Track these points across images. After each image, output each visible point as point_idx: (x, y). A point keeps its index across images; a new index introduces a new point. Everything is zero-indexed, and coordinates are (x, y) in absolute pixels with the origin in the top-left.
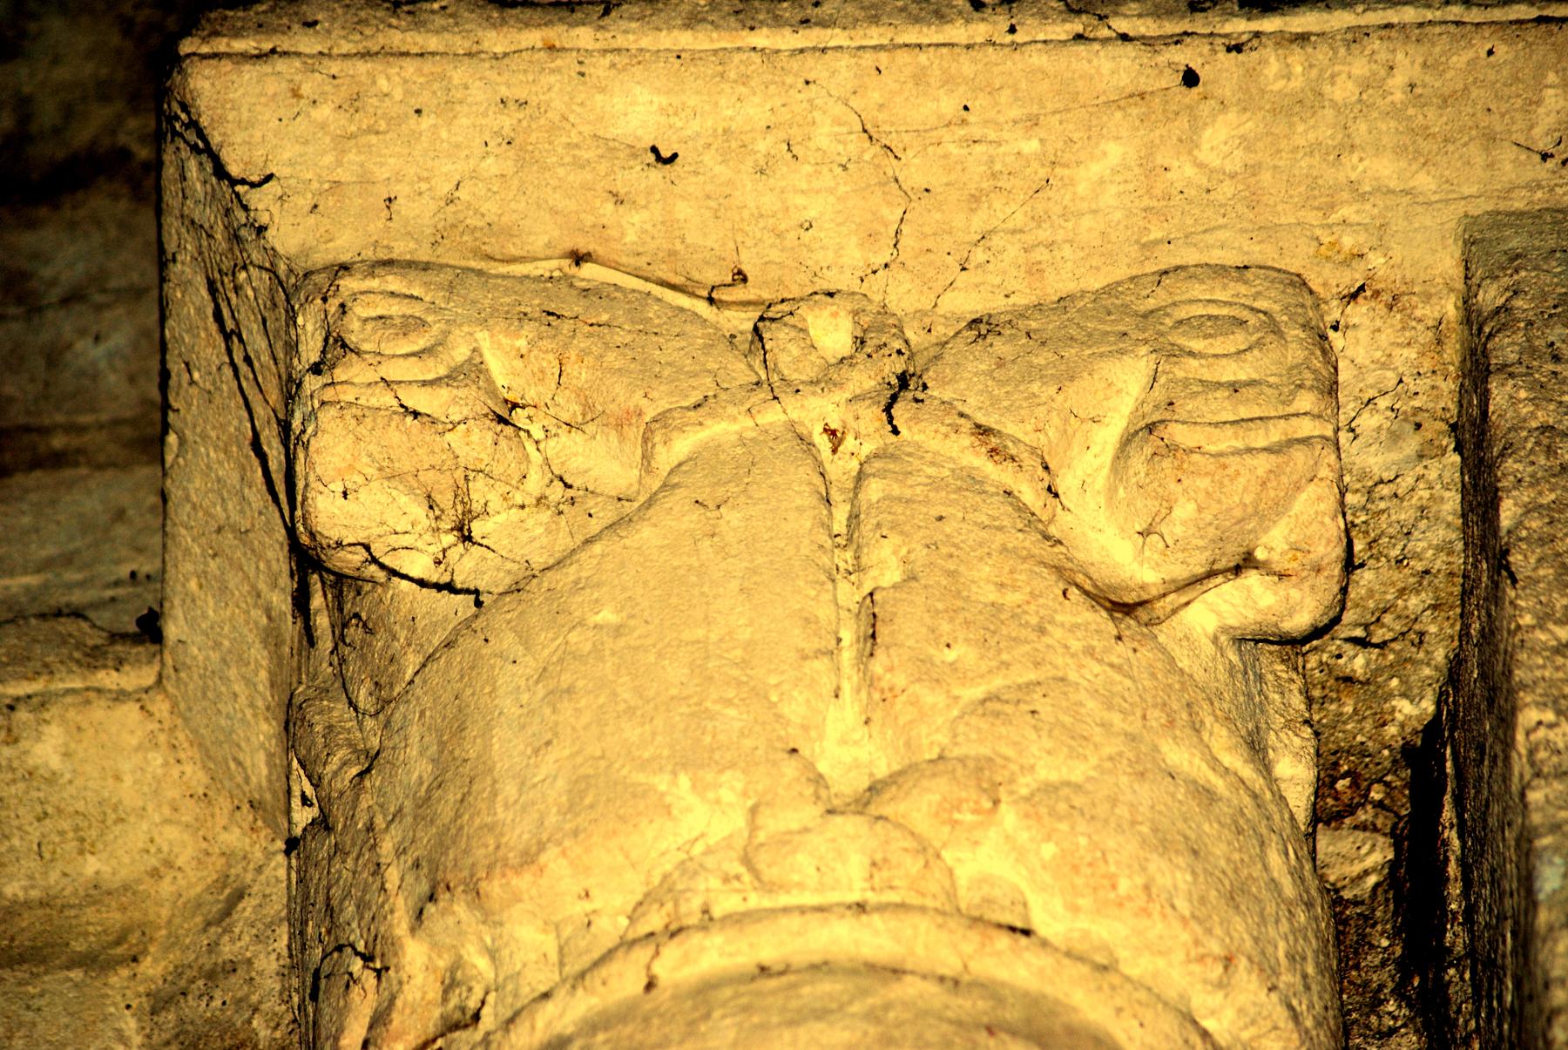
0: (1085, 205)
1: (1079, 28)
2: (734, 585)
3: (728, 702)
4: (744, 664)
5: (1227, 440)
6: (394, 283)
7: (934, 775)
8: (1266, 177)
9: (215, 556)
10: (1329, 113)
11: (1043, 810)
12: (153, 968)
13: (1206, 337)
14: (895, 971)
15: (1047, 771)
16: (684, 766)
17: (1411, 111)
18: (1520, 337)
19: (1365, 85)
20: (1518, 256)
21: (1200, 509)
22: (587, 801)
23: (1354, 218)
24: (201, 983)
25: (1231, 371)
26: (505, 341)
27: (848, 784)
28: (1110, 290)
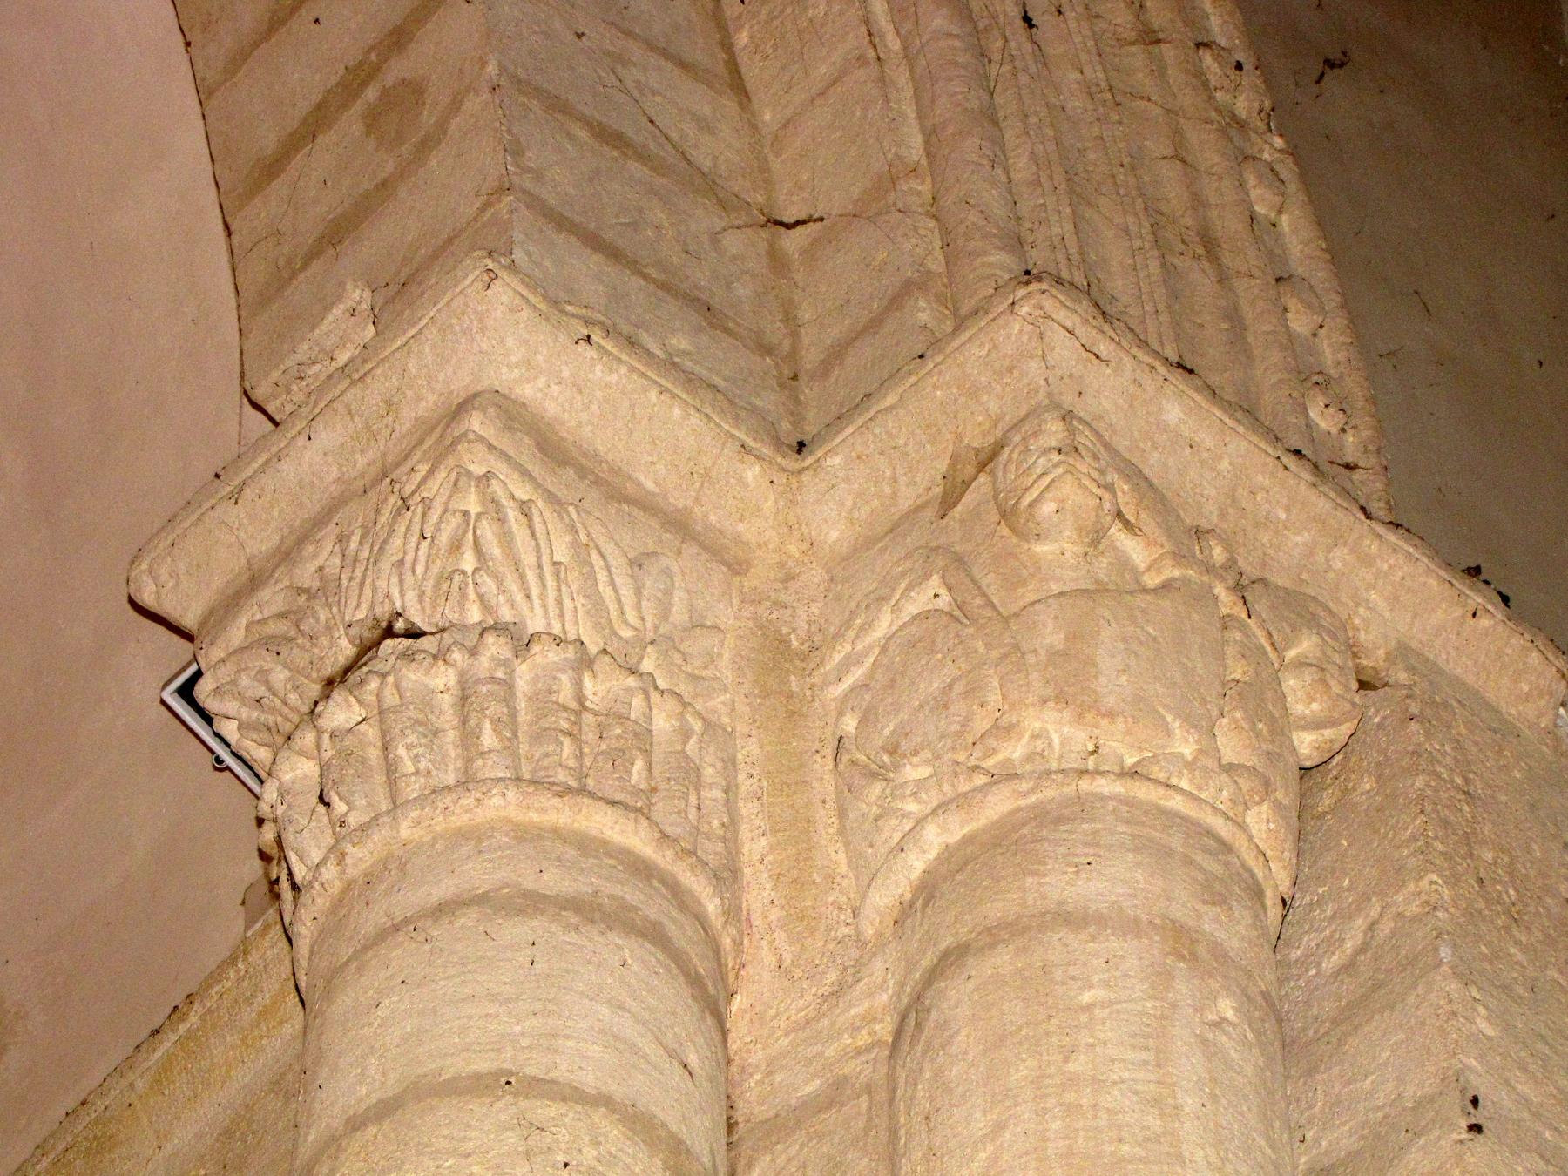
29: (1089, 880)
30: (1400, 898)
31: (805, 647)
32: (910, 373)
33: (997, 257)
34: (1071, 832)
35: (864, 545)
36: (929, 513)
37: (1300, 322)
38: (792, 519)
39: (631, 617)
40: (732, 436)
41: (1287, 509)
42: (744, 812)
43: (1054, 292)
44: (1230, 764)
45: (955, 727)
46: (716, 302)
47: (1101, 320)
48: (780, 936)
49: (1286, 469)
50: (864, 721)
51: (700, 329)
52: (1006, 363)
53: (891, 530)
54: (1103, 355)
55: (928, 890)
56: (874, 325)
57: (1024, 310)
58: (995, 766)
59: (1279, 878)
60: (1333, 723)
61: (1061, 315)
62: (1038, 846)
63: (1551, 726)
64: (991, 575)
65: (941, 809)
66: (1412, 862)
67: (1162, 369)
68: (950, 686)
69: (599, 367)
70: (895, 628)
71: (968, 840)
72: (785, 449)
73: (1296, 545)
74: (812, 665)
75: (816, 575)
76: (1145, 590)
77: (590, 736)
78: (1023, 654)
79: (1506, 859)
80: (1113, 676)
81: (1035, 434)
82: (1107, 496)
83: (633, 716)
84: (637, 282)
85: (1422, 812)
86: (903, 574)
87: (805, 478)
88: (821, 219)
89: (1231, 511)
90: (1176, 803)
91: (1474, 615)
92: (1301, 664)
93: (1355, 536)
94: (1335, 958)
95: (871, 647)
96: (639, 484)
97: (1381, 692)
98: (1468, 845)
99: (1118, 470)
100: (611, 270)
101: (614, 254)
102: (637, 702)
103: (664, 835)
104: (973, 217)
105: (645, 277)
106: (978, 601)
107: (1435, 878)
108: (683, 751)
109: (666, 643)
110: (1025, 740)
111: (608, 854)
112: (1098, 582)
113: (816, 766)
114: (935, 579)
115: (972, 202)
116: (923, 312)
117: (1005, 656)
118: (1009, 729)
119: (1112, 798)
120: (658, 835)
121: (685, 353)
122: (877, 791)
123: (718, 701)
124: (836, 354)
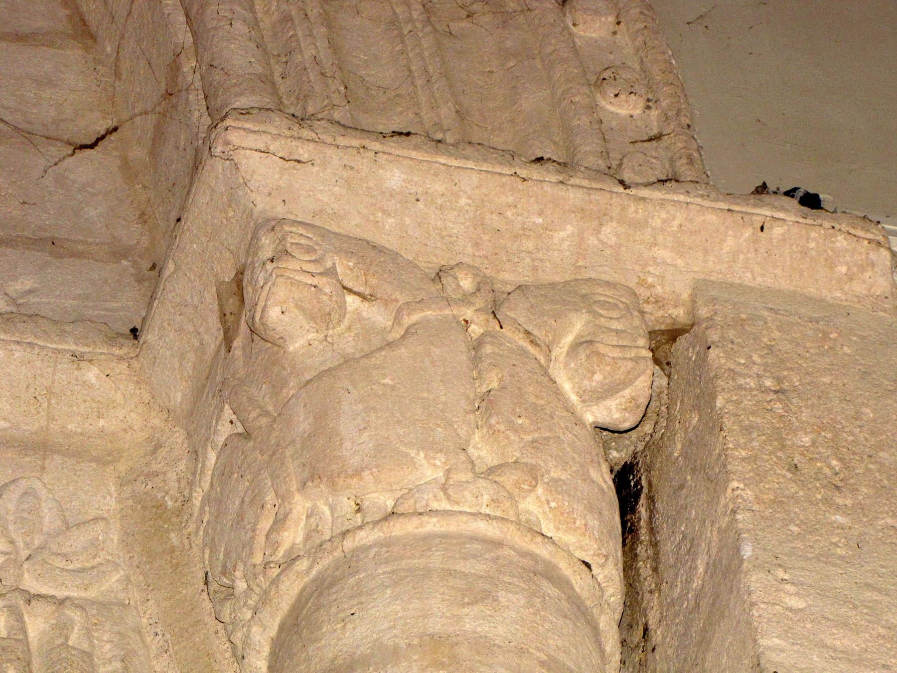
0: (555, 247)
1: (561, 179)
2: (438, 378)
3: (438, 426)
4: (443, 411)
5: (616, 353)
6: (301, 231)
7: (516, 469)
8: (623, 249)
9: (181, 315)
10: (649, 230)
11: (553, 489)
12: (122, 467)
13: (607, 310)
14: (500, 544)
15: (554, 474)
16: (423, 448)
17: (679, 235)
18: (719, 332)
19: (664, 221)
20: (714, 299)
21: (605, 378)
22: (382, 455)
23: (653, 271)
24: (142, 478)
25: (615, 325)
26: (345, 262)
27: (480, 468)
28: (567, 283)
31: (179, 504)
35: (198, 394)
40: (59, 351)
41: (540, 213)
47: (296, 127)
54: (305, 157)
58: (283, 557)
73: (563, 239)
74: (186, 517)
90: (432, 525)
99: (337, 252)
119: (376, 544)
121: (31, 292)
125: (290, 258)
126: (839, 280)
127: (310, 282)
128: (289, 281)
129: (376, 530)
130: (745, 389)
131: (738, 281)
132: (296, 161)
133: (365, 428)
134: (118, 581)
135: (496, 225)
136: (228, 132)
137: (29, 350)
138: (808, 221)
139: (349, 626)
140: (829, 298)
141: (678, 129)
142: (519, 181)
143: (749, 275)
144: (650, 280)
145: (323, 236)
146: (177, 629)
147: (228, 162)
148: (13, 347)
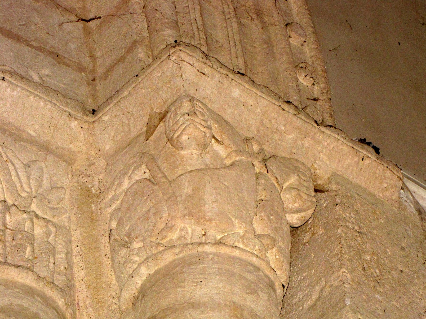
3: (244, 210)
21: (299, 206)
29: (201, 288)
30: (332, 278)
31: (98, 192)
32: (133, 82)
33: (169, 32)
34: (195, 269)
36: (142, 138)
37: (295, 41)
38: (91, 141)
39: (26, 188)
40: (65, 111)
41: (285, 126)
42: (75, 261)
43: (185, 50)
44: (259, 235)
45: (151, 227)
46: (60, 52)
47: (205, 58)
48: (90, 309)
49: (283, 110)
50: (119, 224)
51: (54, 65)
52: (168, 79)
53: (128, 145)
54: (206, 73)
55: (143, 292)
56: (122, 59)
57: (173, 58)
58: (166, 242)
59: (282, 276)
60: (305, 210)
61: (188, 59)
62: (182, 275)
63: (397, 198)
64: (165, 164)
65: (146, 261)
66: (336, 264)
67: (231, 76)
68: (149, 211)
69: (9, 90)
70: (130, 185)
71: (157, 272)
72: (87, 113)
73: (289, 139)
74: (100, 200)
75: (102, 162)
76: (225, 167)
77: (9, 238)
78: (176, 197)
79: (376, 258)
80: (210, 207)
81: (180, 107)
82: (207, 131)
83: (26, 230)
84: (27, 49)
85: (340, 244)
86: (133, 163)
87: (95, 125)
88: (100, 18)
89: (262, 128)
90: (236, 253)
91: (363, 159)
92: (290, 188)
93: (313, 133)
94: (309, 302)
95: (121, 193)
96: (28, 133)
97: (326, 193)
98: (360, 254)
99: (213, 119)
100: (17, 46)
101: (17, 38)
102: (28, 224)
103: (39, 277)
104: (158, 15)
105: (31, 46)
106: (160, 175)
107: (344, 270)
108: (47, 241)
109: (42, 198)
110: (178, 231)
111: (16, 287)
112: (206, 165)
113: (103, 241)
114: (144, 166)
115: (158, 9)
116: (141, 53)
117: (170, 198)
118: (171, 227)
119: (211, 253)
120: (36, 277)
121: (47, 76)
122: (124, 252)
123: (64, 218)
124: (110, 70)
125: (196, 116)
126: (383, 189)
127: (202, 129)
128: (195, 127)
129: (213, 247)
130: (348, 228)
131: (347, 178)
132: (203, 73)
133: (215, 202)
134: (66, 217)
135: (267, 125)
136: (181, 52)
137: (53, 106)
138: (378, 161)
139: (199, 286)
140: (377, 196)
141: (327, 99)
142: (281, 110)
143: (352, 176)
144: (316, 166)
145: (208, 110)
146: (87, 247)
147: (176, 64)
148: (48, 103)
